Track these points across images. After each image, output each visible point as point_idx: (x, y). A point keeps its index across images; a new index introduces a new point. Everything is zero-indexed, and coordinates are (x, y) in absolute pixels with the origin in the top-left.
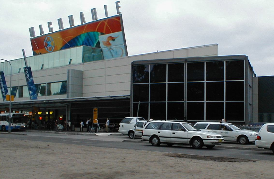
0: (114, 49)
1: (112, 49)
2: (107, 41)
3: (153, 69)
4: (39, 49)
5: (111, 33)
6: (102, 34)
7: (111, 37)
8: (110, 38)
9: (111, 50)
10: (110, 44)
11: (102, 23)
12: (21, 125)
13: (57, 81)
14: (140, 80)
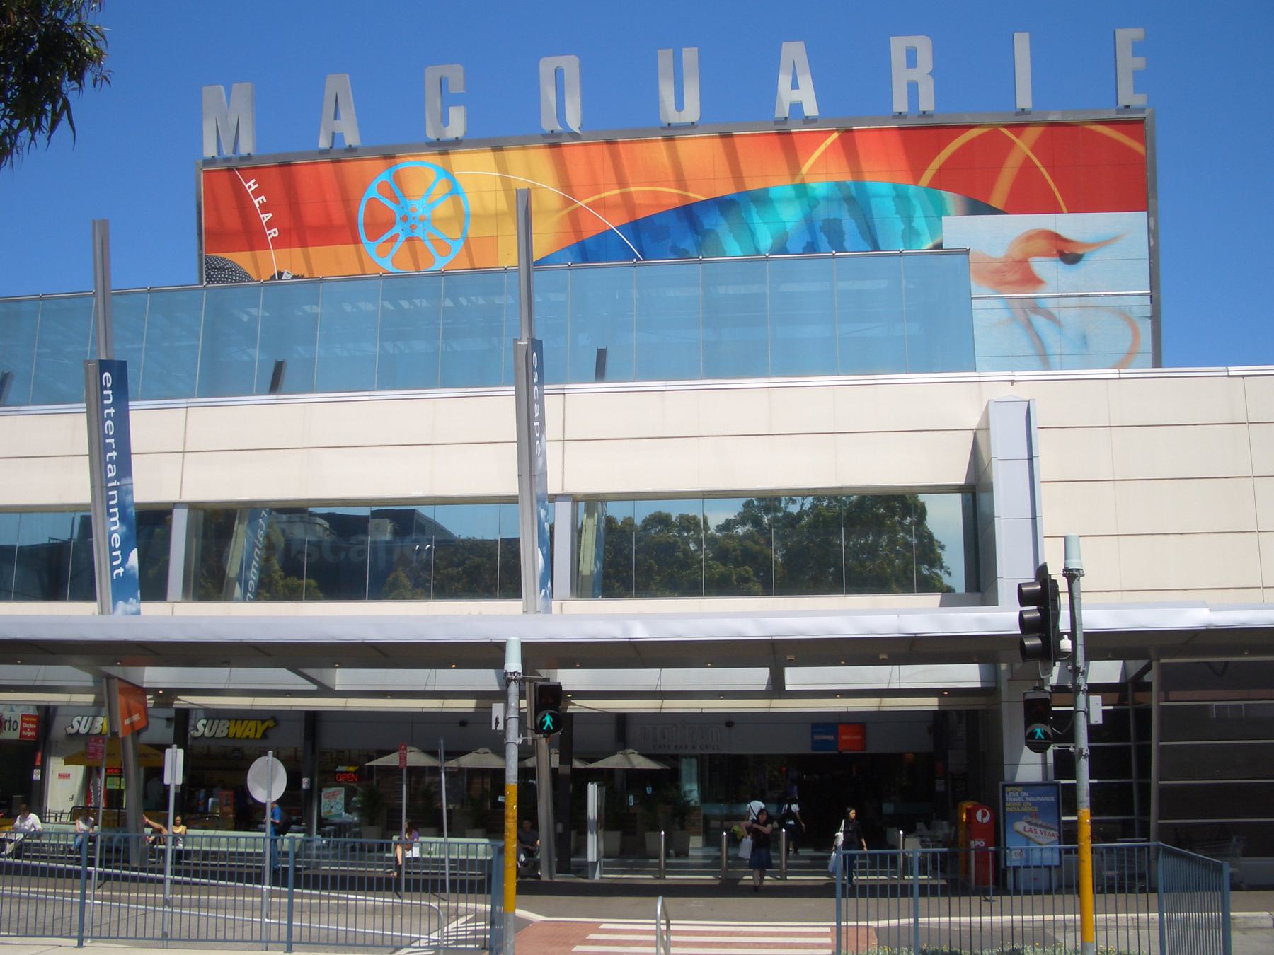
0: (1069, 316)
1: (1050, 316)
2: (1017, 255)
3: (692, 516)
4: (278, 243)
5: (1056, 210)
6: (978, 206)
7: (1055, 237)
8: (1042, 244)
9: (1039, 321)
10: (1032, 280)
11: (1031, 151)
12: (497, 719)
13: (577, 438)
14: (457, 561)
